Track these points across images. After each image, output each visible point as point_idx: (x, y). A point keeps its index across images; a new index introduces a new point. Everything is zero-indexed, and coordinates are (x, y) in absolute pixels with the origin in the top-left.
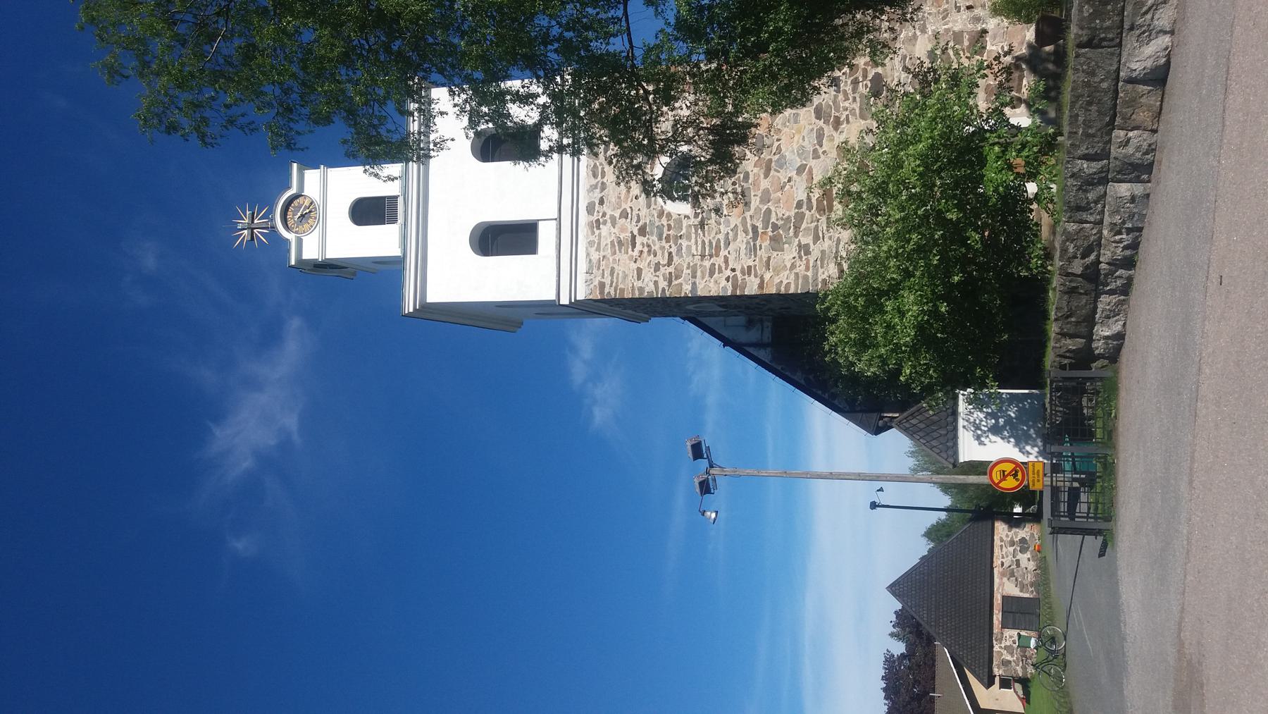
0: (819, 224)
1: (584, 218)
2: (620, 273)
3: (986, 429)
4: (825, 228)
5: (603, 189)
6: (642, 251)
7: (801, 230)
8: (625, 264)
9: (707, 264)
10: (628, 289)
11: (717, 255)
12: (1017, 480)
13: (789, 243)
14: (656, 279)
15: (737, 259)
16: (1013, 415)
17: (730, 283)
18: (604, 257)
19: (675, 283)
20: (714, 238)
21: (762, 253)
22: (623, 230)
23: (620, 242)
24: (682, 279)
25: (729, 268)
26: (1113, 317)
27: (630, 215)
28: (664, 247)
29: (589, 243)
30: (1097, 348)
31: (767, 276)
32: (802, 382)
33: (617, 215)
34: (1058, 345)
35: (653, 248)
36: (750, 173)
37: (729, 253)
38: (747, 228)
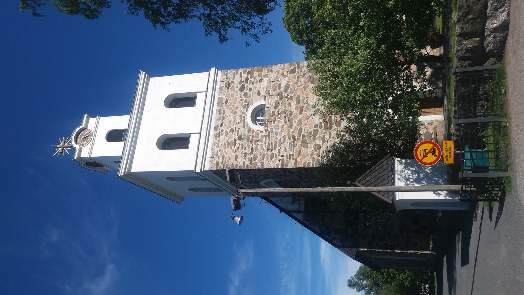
0: (325, 135)
1: (212, 132)
2: (227, 157)
3: (412, 180)
4: (328, 137)
5: (223, 119)
6: (239, 147)
7: (316, 138)
8: (230, 153)
9: (270, 153)
10: (230, 165)
11: (275, 149)
12: (435, 156)
13: (310, 144)
14: (244, 160)
15: (285, 151)
16: (429, 171)
17: (280, 162)
18: (220, 150)
19: (253, 162)
20: (274, 141)
21: (297, 148)
22: (230, 138)
23: (229, 143)
24: (257, 160)
25: (280, 155)
26: (501, 8)
27: (234, 131)
28: (250, 145)
29: (213, 143)
30: (488, 46)
31: (299, 159)
32: (319, 231)
33: (228, 131)
34: (460, 48)
35: (244, 146)
36: (293, 112)
37: (281, 148)
38: (290, 137)
